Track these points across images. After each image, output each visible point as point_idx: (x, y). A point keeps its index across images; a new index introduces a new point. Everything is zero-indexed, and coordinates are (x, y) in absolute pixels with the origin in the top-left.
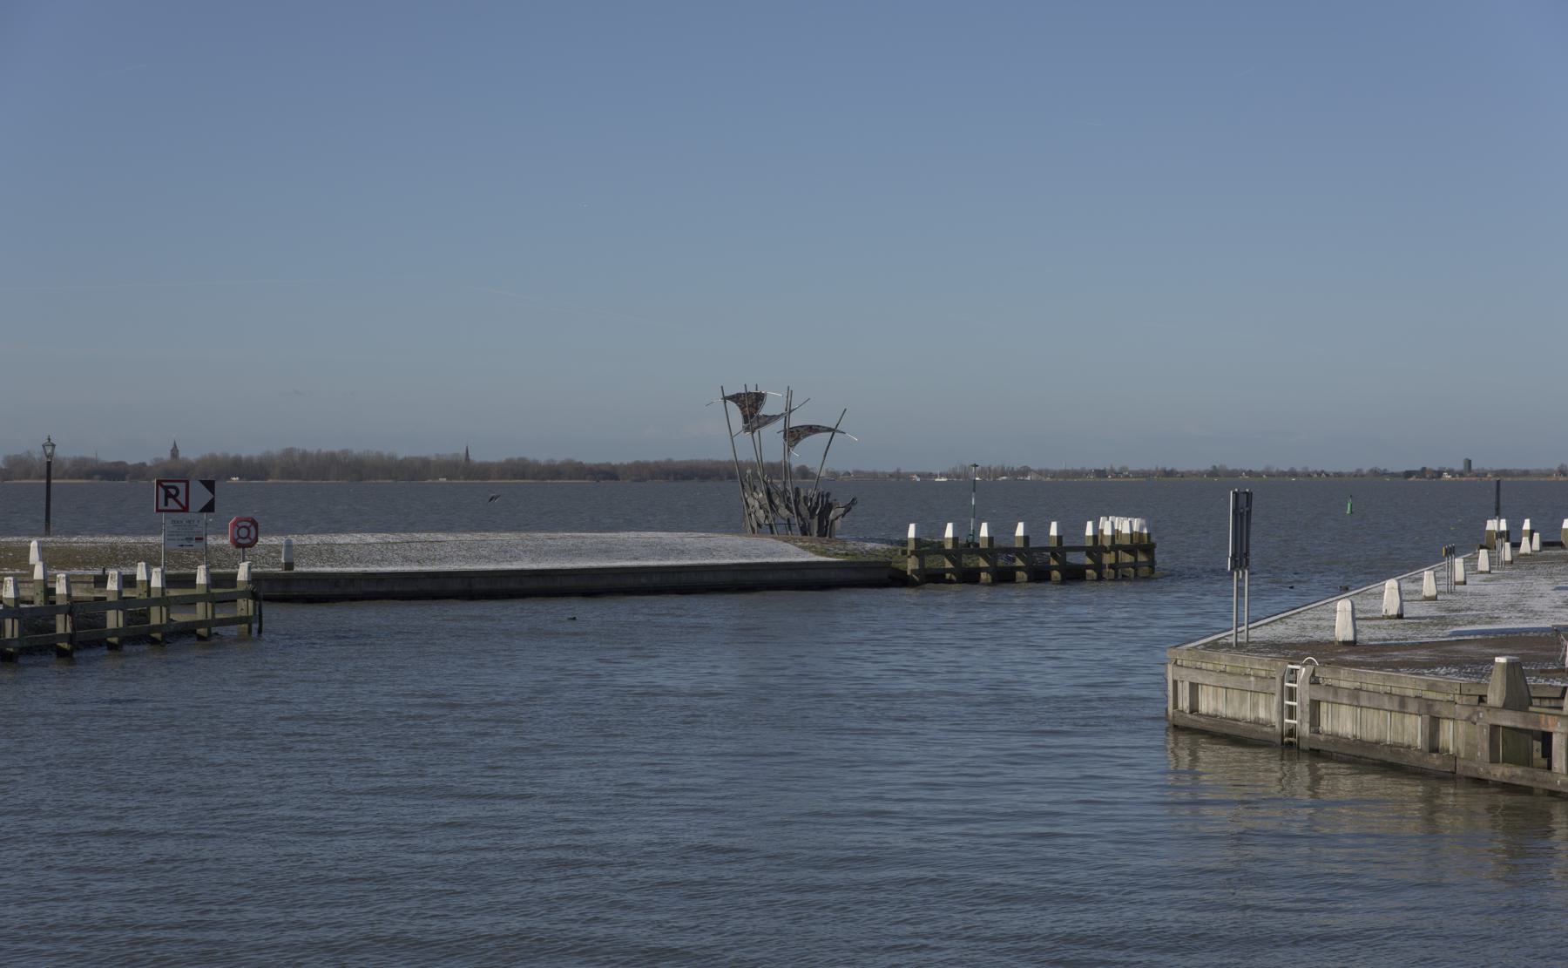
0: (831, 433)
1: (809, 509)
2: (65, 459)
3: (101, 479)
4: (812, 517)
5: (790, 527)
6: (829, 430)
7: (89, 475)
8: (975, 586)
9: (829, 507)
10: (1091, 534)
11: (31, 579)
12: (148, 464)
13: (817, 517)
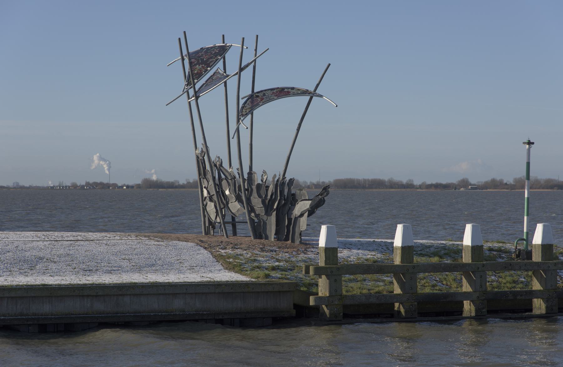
0: (307, 98)
1: (263, 202)
2: (541, 179)
3: (558, 189)
4: (268, 213)
5: (234, 226)
6: (305, 92)
7: (552, 187)
8: (522, 324)
9: (293, 200)
10: (324, 246)
11: (317, 247)
12: (105, 183)
13: (274, 213)
